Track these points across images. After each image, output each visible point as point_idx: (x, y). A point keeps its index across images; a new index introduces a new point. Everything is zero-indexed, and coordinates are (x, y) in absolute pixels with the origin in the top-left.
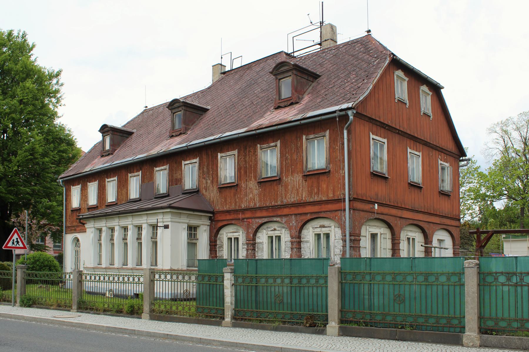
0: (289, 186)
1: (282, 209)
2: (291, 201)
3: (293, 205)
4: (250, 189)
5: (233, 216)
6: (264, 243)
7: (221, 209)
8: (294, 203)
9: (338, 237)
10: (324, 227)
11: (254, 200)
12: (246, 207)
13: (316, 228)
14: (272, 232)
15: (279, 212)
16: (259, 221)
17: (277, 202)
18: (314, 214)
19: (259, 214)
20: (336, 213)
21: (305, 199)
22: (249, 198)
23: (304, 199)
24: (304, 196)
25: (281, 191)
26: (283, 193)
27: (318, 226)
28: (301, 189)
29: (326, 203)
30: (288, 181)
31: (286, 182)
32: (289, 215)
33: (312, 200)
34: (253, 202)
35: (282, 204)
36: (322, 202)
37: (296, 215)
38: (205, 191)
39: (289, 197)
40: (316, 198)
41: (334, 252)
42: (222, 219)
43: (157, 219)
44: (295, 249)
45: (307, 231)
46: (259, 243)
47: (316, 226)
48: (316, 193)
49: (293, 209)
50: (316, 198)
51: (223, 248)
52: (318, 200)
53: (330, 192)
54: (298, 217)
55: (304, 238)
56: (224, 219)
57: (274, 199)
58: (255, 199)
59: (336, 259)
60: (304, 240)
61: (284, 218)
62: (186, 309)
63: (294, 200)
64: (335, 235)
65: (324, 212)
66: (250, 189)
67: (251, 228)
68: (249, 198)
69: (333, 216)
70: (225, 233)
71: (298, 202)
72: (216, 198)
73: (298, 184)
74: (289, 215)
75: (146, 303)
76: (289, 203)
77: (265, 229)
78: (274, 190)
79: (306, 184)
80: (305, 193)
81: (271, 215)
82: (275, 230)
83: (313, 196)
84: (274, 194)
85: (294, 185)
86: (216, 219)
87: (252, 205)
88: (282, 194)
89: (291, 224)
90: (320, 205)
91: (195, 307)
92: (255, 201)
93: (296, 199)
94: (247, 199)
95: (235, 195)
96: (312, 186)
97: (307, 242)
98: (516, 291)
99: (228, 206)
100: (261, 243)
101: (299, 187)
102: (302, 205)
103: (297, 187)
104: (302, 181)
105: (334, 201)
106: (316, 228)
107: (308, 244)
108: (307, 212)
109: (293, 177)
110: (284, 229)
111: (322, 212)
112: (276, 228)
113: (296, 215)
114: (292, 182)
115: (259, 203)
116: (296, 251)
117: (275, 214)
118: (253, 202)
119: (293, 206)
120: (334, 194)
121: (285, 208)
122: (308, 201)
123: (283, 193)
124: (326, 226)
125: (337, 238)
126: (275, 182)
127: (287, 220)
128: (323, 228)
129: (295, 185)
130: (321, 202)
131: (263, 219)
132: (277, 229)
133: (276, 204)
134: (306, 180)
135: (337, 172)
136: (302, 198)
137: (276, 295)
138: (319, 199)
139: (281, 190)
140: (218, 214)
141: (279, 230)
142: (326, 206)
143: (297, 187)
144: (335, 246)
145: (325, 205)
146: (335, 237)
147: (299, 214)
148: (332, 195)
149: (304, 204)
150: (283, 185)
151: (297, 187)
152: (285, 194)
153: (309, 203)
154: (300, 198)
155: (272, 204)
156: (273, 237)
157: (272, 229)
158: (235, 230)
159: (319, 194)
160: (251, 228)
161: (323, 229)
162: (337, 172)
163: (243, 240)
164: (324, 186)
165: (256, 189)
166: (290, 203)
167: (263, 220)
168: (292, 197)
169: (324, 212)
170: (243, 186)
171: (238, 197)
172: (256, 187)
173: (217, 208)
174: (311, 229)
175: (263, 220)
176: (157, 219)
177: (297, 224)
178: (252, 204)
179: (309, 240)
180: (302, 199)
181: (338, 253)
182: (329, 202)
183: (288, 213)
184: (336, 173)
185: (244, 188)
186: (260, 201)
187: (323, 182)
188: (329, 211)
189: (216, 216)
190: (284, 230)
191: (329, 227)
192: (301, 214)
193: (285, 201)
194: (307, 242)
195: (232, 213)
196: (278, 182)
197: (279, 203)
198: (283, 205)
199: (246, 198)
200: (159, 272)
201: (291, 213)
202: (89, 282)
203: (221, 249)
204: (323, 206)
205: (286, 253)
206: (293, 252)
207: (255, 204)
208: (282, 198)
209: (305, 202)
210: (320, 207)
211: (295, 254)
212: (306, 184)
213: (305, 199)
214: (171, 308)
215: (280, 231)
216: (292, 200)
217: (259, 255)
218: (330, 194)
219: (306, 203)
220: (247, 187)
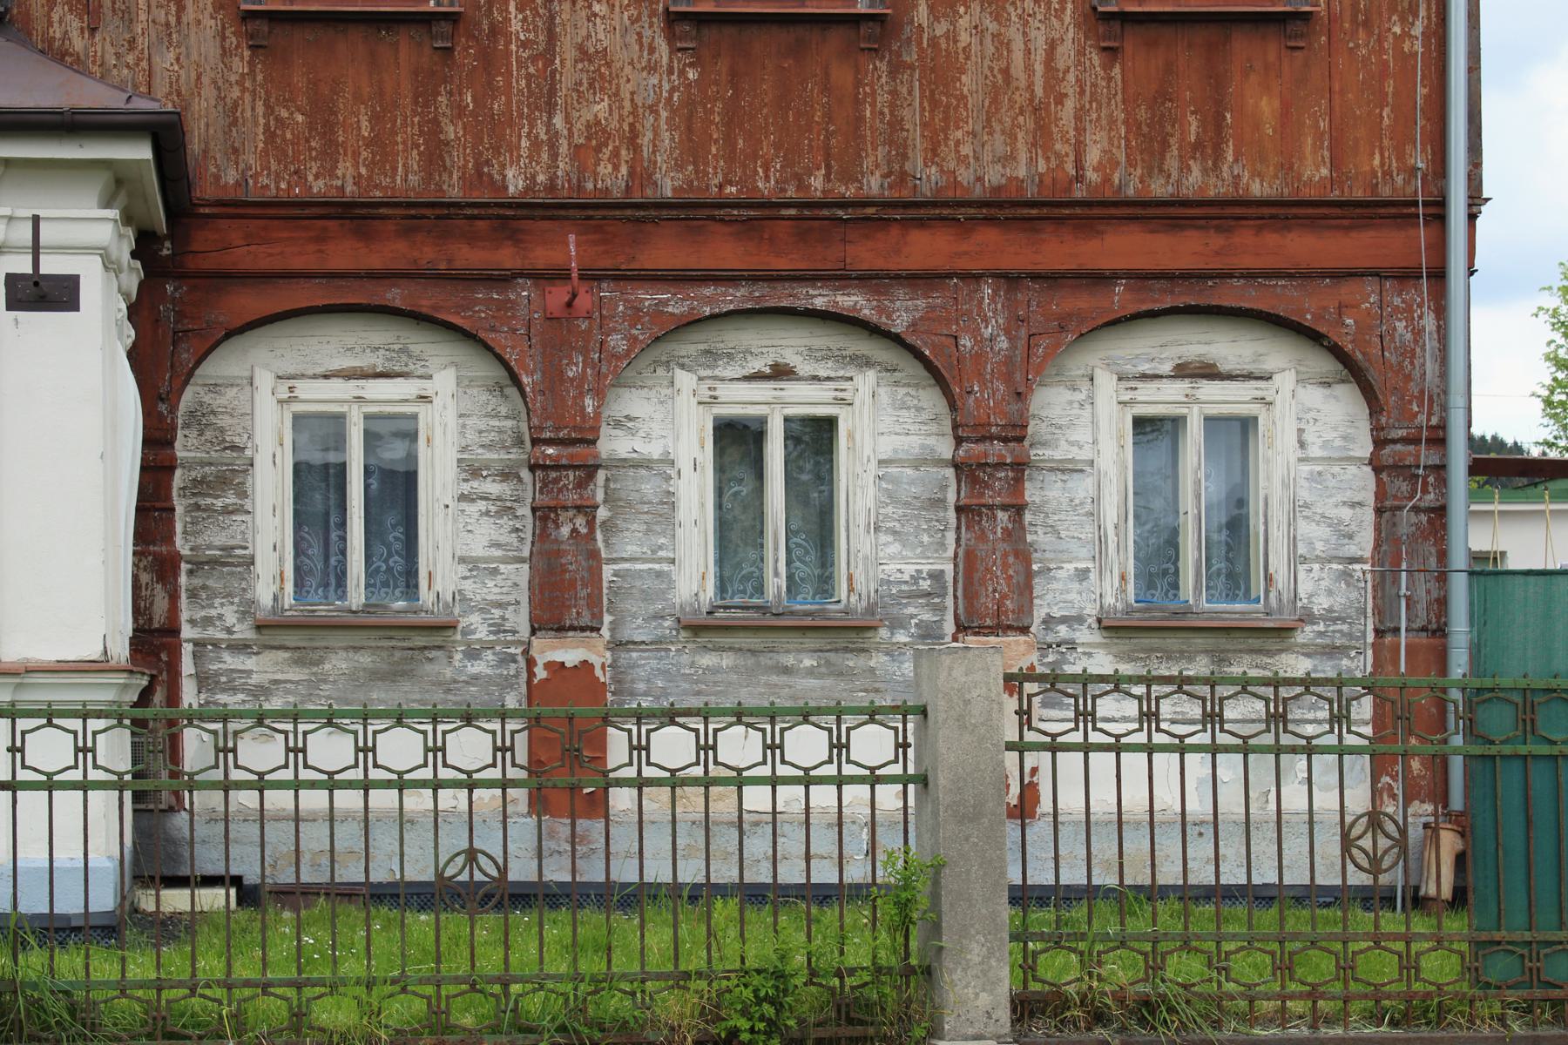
0: (963, 71)
1: (895, 231)
2: (979, 179)
3: (1001, 214)
4: (584, 54)
5: (401, 246)
6: (685, 464)
7: (272, 184)
8: (1014, 196)
9: (1326, 444)
10: (1209, 372)
11: (633, 139)
12: (551, 186)
13: (1144, 377)
14: (763, 391)
15: (865, 253)
16: (666, 303)
17: (848, 177)
18: (1163, 284)
19: (664, 252)
20: (1347, 290)
21: (1107, 180)
22: (579, 126)
23: (1092, 176)
24: (1093, 156)
25: (893, 107)
26: (912, 116)
27: (1166, 368)
28: (1070, 104)
29: (1272, 217)
30: (952, 36)
31: (934, 42)
32: (949, 276)
33: (1159, 189)
34: (616, 154)
35: (905, 194)
36: (1238, 211)
37: (1010, 280)
38: (74, 24)
39: (966, 150)
40: (1195, 175)
41: (1293, 541)
42: (265, 264)
43: (36, 220)
44: (1000, 514)
45: (1068, 395)
46: (624, 463)
47: (1145, 368)
48: (1198, 146)
49: (988, 237)
50: (1195, 181)
51: (243, 494)
52: (1211, 193)
53: (1308, 149)
54: (1030, 295)
55: (1044, 444)
56: (297, 264)
57: (828, 156)
58: (645, 140)
59: (1304, 588)
60: (1048, 453)
61: (900, 293)
62: (1318, 967)
63: (1010, 179)
64: (1301, 431)
65: (1250, 275)
66: (584, 54)
67: (585, 352)
68: (579, 126)
69: (1325, 308)
70: (264, 380)
71: (1047, 196)
72: (208, 92)
73: (1039, 68)
74: (949, 276)
75: (976, 952)
76: (959, 195)
77: (682, 367)
78: (826, 89)
79: (1110, 79)
80: (1101, 136)
81: (782, 264)
82: (781, 373)
83: (1172, 164)
84: (829, 117)
85: (1006, 72)
86: (208, 263)
87: (610, 177)
88: (896, 124)
89: (966, 342)
90: (1218, 229)
91: (1464, 947)
92: (636, 148)
93: (1022, 172)
94: (554, 136)
95: (424, 97)
96: (1162, 96)
97: (1068, 469)
98: (435, 757)
99: (345, 168)
100: (645, 464)
101: (1048, 87)
102: (1069, 217)
103: (1030, 87)
104: (1081, 53)
105: (1337, 211)
106: (1144, 377)
107: (1082, 487)
108: (1106, 264)
109: (997, 18)
110: (871, 375)
111: (1231, 276)
112: (791, 358)
113: (1010, 280)
114: (990, 49)
115: (679, 167)
116: (1005, 530)
117: (828, 257)
118: (616, 154)
119: (989, 220)
120: (1335, 164)
121: (921, 223)
122: (1131, 192)
123: (912, 116)
124: (1224, 367)
125: (1315, 451)
126: (836, 36)
127: (931, 308)
128: (1204, 383)
129: (1018, 69)
130: (1229, 211)
131: (708, 291)
132: (804, 368)
133: (849, 192)
134: (1111, 53)
135: (1367, 24)
136: (1079, 165)
137: (1348, 819)
138: (1217, 189)
139: (894, 93)
140: (223, 223)
141: (815, 378)
142: (1271, 239)
143: (1039, 91)
144: (1297, 509)
145: (1260, 229)
146: (1302, 444)
147: (1035, 276)
148: (1325, 172)
149: (1096, 211)
150: (910, 57)
151: (1039, 91)
152: (924, 125)
153: (1140, 211)
154: (1060, 166)
155: (802, 186)
156: (340, 419)
157: (759, 365)
158: (378, 361)
159: (1218, 157)
160: (585, 352)
161: (1210, 390)
162: (1367, 24)
163: (462, 434)
164: (1267, 107)
165: (652, 68)
166: (978, 193)
167: (710, 300)
168: (987, 157)
169: (1250, 275)
170: (515, 26)
171: (460, 111)
172: (652, 50)
173: (231, 176)
174: (1106, 383)
175: (710, 300)
176: (36, 220)
177: (1022, 343)
178: (605, 169)
179: (1085, 454)
180: (1079, 178)
181: (1320, 546)
182: (1296, 217)
183: (939, 263)
184: (1354, 33)
185: (524, 45)
186: (692, 150)
187: (1253, 78)
188: (1290, 276)
189: (203, 239)
190: (866, 381)
191: (1249, 376)
192: (1051, 279)
193: (928, 179)
194: (1068, 469)
195: (390, 226)
196: (869, 38)
197: (874, 185)
198: (907, 205)
199: (549, 125)
200: (1138, 680)
201: (974, 266)
202: (69, 802)
203: (219, 503)
204: (1245, 238)
205: (884, 538)
206: (982, 537)
207: (641, 174)
208: (905, 157)
209: (1109, 195)
210: (1216, 241)
211: (1001, 546)
212: (1110, 79)
213: (1107, 180)
214: (1410, 966)
215: (832, 385)
216: (994, 175)
217: (631, 549)
218: (1309, 161)
219: (1115, 204)
220: (552, 37)
